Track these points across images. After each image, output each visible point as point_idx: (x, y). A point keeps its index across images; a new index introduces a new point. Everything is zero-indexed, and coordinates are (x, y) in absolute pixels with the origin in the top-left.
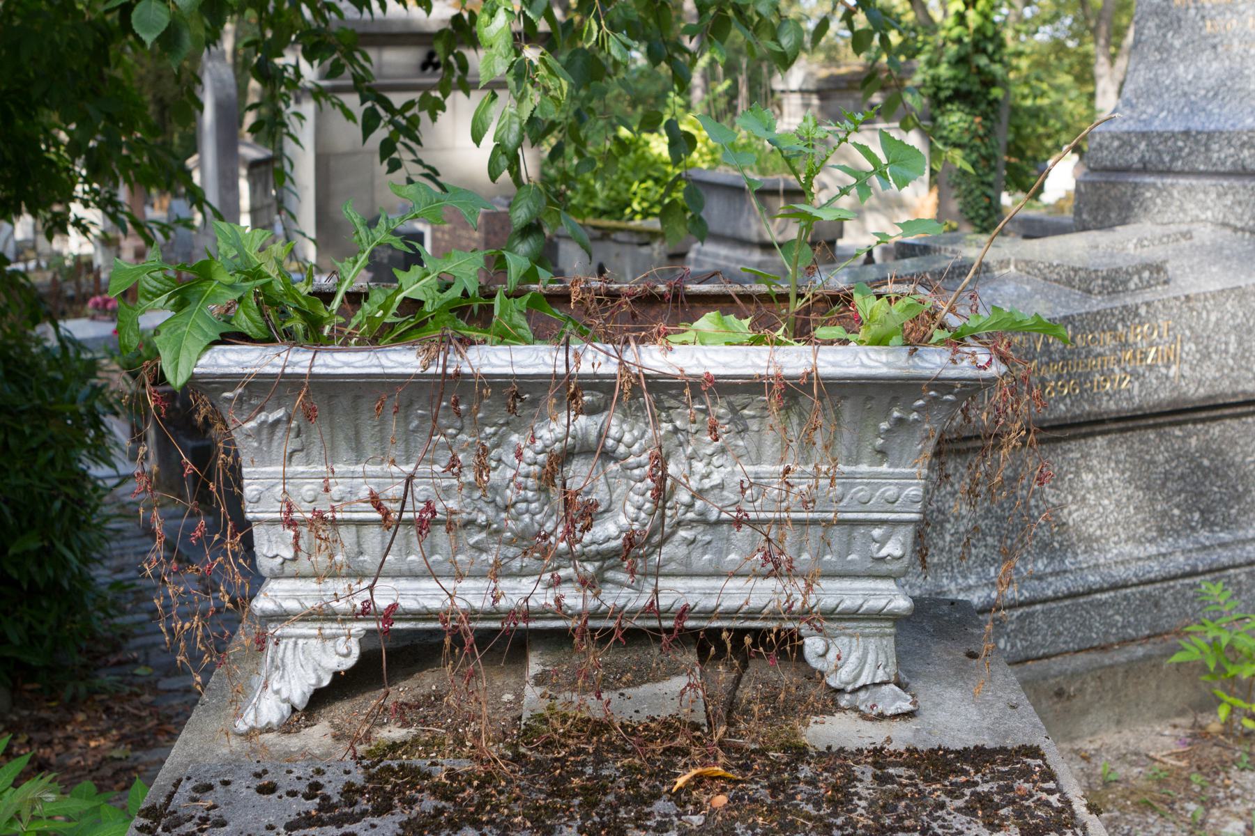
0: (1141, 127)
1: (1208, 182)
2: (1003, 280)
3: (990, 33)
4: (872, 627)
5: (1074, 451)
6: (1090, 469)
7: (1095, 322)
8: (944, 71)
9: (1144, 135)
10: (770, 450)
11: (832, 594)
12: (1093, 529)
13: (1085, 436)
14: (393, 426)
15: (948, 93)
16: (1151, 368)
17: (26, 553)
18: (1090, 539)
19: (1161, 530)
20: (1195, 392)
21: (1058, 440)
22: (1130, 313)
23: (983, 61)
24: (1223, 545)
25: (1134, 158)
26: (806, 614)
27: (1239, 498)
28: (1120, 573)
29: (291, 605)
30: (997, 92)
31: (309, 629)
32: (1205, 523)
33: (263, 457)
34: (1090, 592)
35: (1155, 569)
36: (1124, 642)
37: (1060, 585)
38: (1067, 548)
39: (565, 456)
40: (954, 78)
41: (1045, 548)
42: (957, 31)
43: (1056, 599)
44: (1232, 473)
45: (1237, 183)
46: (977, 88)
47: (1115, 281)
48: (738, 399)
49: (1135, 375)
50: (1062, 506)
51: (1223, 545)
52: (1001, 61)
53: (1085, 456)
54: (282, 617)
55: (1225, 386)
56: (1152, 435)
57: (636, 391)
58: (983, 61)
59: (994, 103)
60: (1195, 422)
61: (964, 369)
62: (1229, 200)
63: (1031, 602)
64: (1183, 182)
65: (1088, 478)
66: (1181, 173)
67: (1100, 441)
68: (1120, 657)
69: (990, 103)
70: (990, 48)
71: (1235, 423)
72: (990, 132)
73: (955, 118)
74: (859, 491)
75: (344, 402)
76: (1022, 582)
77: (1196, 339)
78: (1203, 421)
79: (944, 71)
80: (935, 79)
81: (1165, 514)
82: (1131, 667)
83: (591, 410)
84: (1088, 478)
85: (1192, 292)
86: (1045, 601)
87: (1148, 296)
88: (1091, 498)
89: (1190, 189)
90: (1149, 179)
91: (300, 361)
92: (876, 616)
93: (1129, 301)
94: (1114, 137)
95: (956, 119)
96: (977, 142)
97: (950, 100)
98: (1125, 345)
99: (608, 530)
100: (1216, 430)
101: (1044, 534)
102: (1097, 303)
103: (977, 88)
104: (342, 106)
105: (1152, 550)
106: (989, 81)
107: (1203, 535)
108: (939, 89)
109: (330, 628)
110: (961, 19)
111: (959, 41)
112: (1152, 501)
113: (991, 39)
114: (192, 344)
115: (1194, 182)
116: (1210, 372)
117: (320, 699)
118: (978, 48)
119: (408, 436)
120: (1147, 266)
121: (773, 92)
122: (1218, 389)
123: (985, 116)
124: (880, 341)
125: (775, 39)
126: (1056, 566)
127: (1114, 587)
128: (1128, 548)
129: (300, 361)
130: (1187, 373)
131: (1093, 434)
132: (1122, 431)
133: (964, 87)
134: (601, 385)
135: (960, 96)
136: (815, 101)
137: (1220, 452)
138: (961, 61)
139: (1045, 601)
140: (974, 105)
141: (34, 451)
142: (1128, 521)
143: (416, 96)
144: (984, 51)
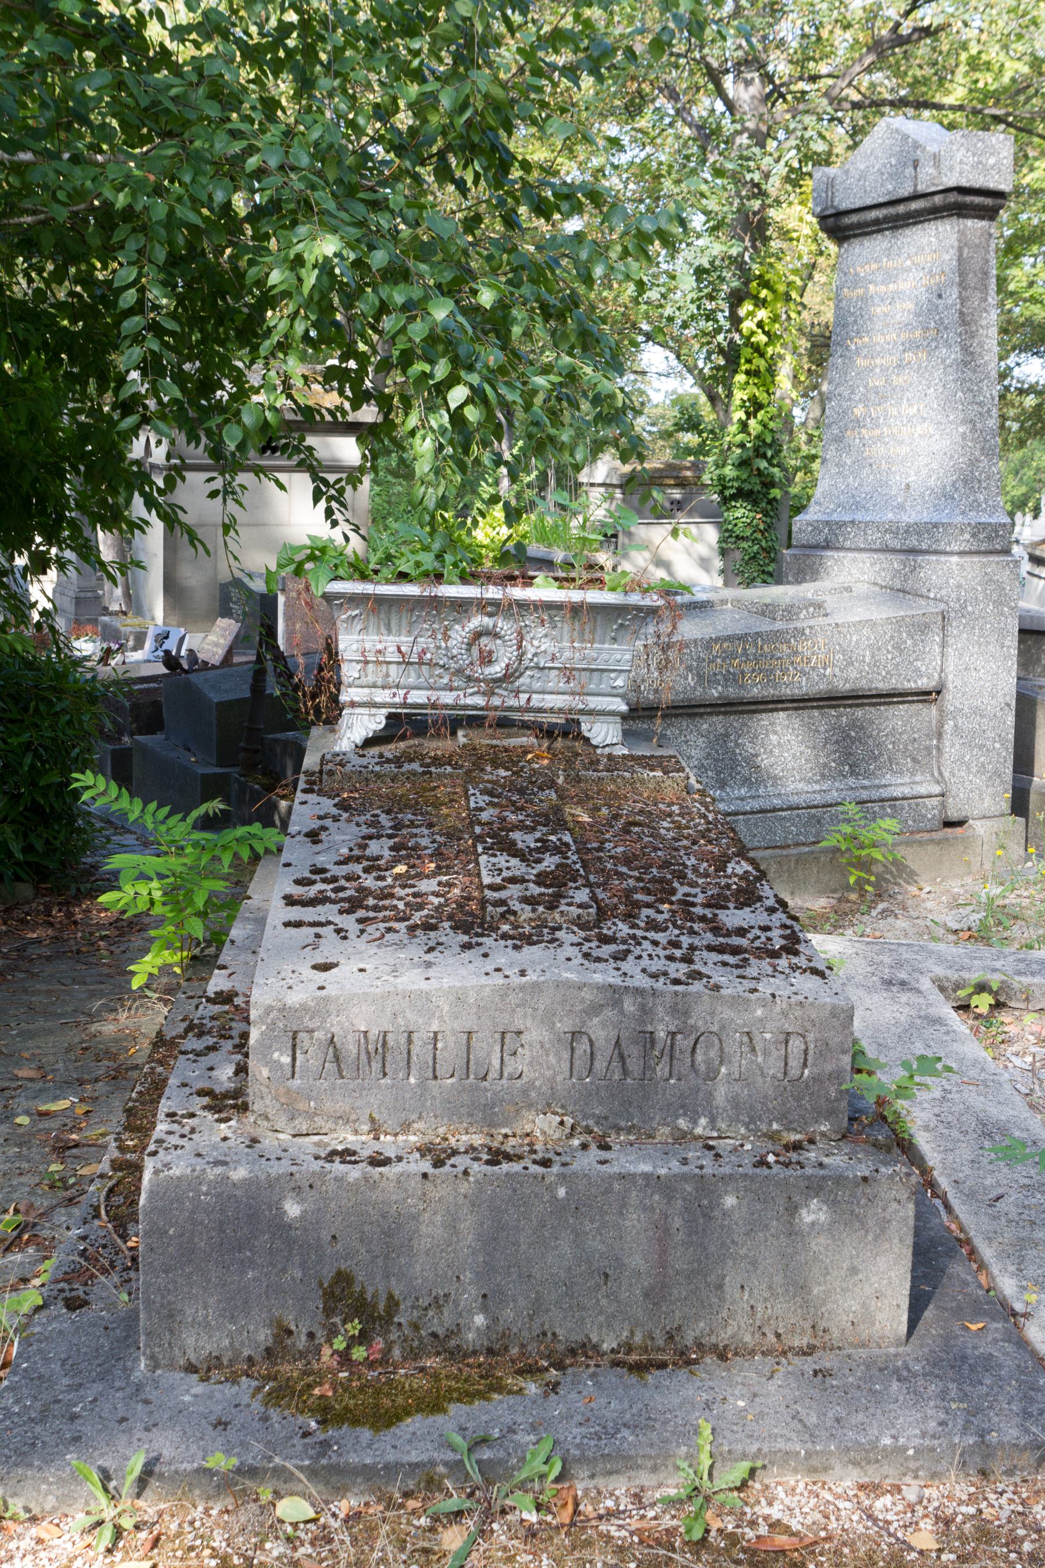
0: (826, 518)
1: (865, 555)
2: (722, 611)
3: (769, 440)
4: (611, 719)
5: (765, 719)
6: (775, 733)
7: (777, 636)
8: (729, 471)
9: (827, 523)
10: (566, 637)
11: (595, 703)
12: (777, 771)
13: (772, 711)
14: (404, 621)
15: (733, 491)
16: (813, 669)
17: (49, 786)
18: (776, 778)
19: (823, 776)
20: (843, 687)
21: (754, 712)
22: (800, 632)
23: (763, 464)
24: (864, 788)
25: (821, 538)
26: (582, 712)
27: (875, 759)
28: (795, 800)
29: (356, 699)
30: (776, 493)
31: (364, 711)
32: (853, 773)
33: (348, 631)
34: (774, 810)
35: (818, 799)
36: (797, 844)
37: (756, 805)
38: (760, 782)
39: (478, 635)
40: (738, 478)
41: (746, 781)
42: (740, 437)
43: (752, 813)
44: (870, 742)
45: (881, 556)
46: (758, 488)
47: (790, 612)
48: (553, 612)
49: (803, 673)
50: (756, 755)
51: (864, 788)
52: (778, 465)
53: (772, 724)
54: (353, 704)
55: (863, 684)
56: (816, 713)
57: (510, 605)
58: (763, 464)
59: (772, 501)
60: (845, 706)
61: (647, 602)
62: (877, 567)
63: (736, 813)
64: (850, 555)
65: (774, 738)
66: (849, 549)
67: (782, 714)
68: (793, 851)
69: (770, 502)
70: (769, 453)
71: (872, 709)
72: (769, 527)
73: (738, 513)
74: (604, 656)
75: (385, 607)
76: (730, 801)
77: (844, 652)
78: (850, 706)
79: (729, 471)
80: (721, 478)
81: (825, 765)
82: (799, 859)
83: (490, 615)
84: (774, 738)
85: (840, 621)
86: (745, 813)
87: (812, 623)
88: (776, 751)
89: (854, 560)
90: (829, 553)
91: (369, 588)
92: (612, 713)
93: (799, 625)
94: (809, 524)
95: (740, 513)
96: (759, 536)
97: (734, 497)
98: (796, 653)
99: (497, 669)
100: (859, 713)
101: (745, 772)
102: (779, 625)
103: (758, 488)
104: (277, 482)
105: (817, 787)
106: (769, 483)
107: (851, 781)
108: (725, 487)
109: (374, 711)
110: (744, 426)
111: (742, 445)
112: (817, 756)
113: (770, 446)
114: (323, 580)
115: (856, 555)
116: (853, 674)
117: (368, 743)
118: (759, 454)
119: (411, 624)
120: (811, 604)
121: (581, 484)
122: (858, 686)
123: (766, 514)
124: (613, 589)
125: (572, 455)
126: (753, 793)
127: (790, 808)
128: (801, 786)
129: (369, 588)
130: (838, 673)
131: (777, 710)
132: (796, 709)
133: (747, 487)
134: (495, 603)
135: (741, 494)
136: (618, 494)
137: (862, 728)
138: (743, 464)
139: (745, 813)
140: (755, 503)
141: (56, 714)
142: (800, 767)
143: (344, 476)
144: (764, 456)
